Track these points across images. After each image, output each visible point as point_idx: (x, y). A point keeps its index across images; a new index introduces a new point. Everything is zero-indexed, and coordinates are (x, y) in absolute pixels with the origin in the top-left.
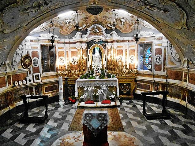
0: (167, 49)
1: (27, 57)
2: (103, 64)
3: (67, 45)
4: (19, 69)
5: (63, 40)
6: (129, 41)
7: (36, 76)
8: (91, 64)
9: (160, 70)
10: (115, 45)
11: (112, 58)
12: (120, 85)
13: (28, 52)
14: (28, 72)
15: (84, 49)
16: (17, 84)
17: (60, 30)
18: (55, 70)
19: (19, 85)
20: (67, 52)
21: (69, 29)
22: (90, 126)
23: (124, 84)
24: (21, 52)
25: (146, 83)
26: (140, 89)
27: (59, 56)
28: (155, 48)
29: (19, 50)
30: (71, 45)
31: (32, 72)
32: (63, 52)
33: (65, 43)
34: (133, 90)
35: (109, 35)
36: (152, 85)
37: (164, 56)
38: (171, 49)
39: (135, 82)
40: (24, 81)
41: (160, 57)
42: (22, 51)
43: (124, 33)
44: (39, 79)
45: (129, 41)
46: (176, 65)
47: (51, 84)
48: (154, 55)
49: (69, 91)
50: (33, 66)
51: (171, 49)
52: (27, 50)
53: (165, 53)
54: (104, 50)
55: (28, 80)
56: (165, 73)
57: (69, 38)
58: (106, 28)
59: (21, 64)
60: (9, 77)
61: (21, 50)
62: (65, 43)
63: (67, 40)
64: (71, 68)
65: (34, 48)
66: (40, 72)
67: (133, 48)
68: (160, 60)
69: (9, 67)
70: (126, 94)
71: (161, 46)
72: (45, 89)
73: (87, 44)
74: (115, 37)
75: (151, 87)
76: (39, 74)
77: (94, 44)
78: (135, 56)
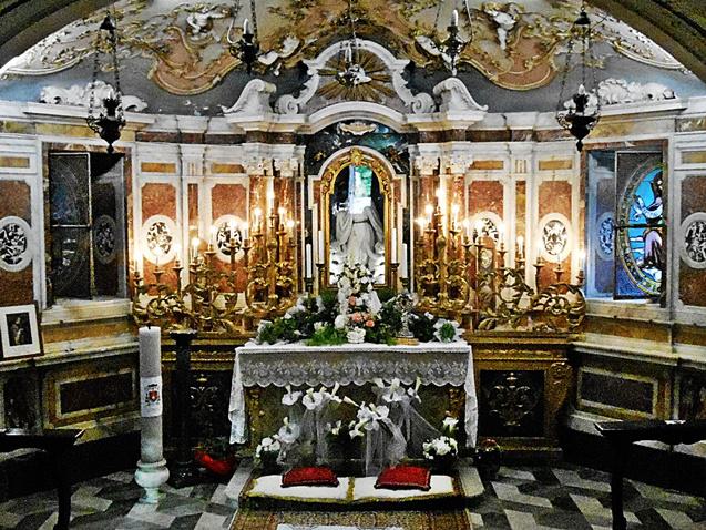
3: (192, 151)
5: (168, 124)
10: (461, 158)
11: (444, 222)
15: (286, 174)
20: (193, 189)
27: (147, 213)
28: (682, 176)
30: (217, 153)
32: (169, 187)
33: (180, 138)
44: (27, 339)
47: (98, 370)
54: (397, 183)
57: (204, 113)
58: (412, 63)
62: (180, 138)
67: (561, 175)
74: (462, 111)
76: (30, 309)
77: (343, 147)
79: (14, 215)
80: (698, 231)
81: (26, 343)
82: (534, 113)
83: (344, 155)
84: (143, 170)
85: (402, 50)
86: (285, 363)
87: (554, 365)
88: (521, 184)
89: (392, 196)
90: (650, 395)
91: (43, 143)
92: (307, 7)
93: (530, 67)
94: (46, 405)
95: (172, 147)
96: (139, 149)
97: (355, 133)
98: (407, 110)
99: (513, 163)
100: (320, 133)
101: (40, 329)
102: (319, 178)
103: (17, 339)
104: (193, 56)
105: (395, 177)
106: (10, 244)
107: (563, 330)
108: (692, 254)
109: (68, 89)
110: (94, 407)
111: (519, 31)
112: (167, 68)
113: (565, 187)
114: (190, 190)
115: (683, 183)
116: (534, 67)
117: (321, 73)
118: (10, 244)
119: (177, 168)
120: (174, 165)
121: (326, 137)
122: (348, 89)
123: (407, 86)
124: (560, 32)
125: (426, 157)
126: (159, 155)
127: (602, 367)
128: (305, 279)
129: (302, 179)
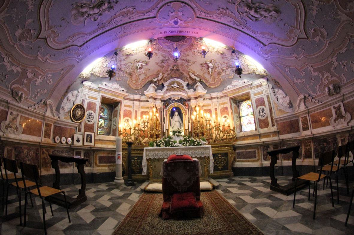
0: (270, 96)
1: (80, 107)
2: (185, 128)
3: (137, 103)
4: (64, 118)
5: (131, 96)
6: (217, 98)
7: (88, 135)
8: (168, 129)
9: (267, 125)
10: (201, 102)
12: (214, 155)
13: (83, 102)
14: (78, 128)
15: (159, 108)
16: (58, 140)
17: (129, 79)
18: (117, 134)
19: (61, 142)
20: (136, 112)
21: (141, 80)
22: (174, 179)
23: (219, 154)
24: (74, 99)
25: (250, 149)
26: (241, 160)
27: (125, 116)
28: (255, 99)
29: (73, 96)
30: (142, 104)
31: (83, 130)
32: (130, 111)
33: (134, 100)
34: (231, 163)
35: (192, 90)
36: (260, 150)
37: (269, 105)
38: (275, 95)
39: (234, 151)
40: (70, 139)
41: (263, 109)
42: (76, 100)
43: (212, 87)
44: (91, 141)
45: (217, 98)
46: (288, 113)
47: (109, 153)
48: (256, 108)
49: (135, 166)
50: (85, 122)
51: (275, 95)
52: (82, 99)
53: (269, 102)
54: (186, 111)
55: (75, 139)
56: (275, 129)
57: (140, 95)
58: (188, 83)
59: (69, 114)
60: (48, 125)
61: (75, 97)
62: (134, 100)
63: (137, 97)
64: (141, 133)
65: (92, 98)
66: (94, 131)
67: (225, 106)
68: (265, 112)
69: (51, 111)
70: (222, 169)
71: (262, 95)
72: (98, 158)
73: (163, 103)
74: (201, 90)
75: (258, 152)
76: (93, 134)
77: (172, 103)
78: (228, 115)
79: (92, 110)
80: (261, 110)
81: (91, 142)
82: (217, 93)
83: (173, 105)
84: (124, 106)
85: (186, 80)
86: (158, 151)
87: (230, 151)
88: (216, 109)
89: (185, 114)
90: (255, 154)
91: (101, 95)
92: (165, 63)
93: (216, 81)
94: (95, 160)
95: (132, 102)
96: (124, 101)
97: (175, 99)
98: (186, 93)
99: (214, 104)
100: (167, 100)
101: (95, 139)
102: (167, 110)
103: (88, 141)
104: (138, 77)
105: (185, 109)
106: (89, 117)
107: (232, 141)
108: (261, 116)
109: (109, 83)
110: (108, 163)
111: (214, 69)
112: (131, 80)
113: (227, 108)
114: (135, 112)
115: (255, 100)
116: (217, 80)
117: (168, 86)
118: (89, 117)
119: (133, 107)
120: (132, 106)
121: (169, 101)
122: (174, 89)
123: (187, 88)
124: (223, 68)
125: (193, 103)
126: (128, 103)
127: (242, 149)
128: (164, 132)
129: (163, 110)
